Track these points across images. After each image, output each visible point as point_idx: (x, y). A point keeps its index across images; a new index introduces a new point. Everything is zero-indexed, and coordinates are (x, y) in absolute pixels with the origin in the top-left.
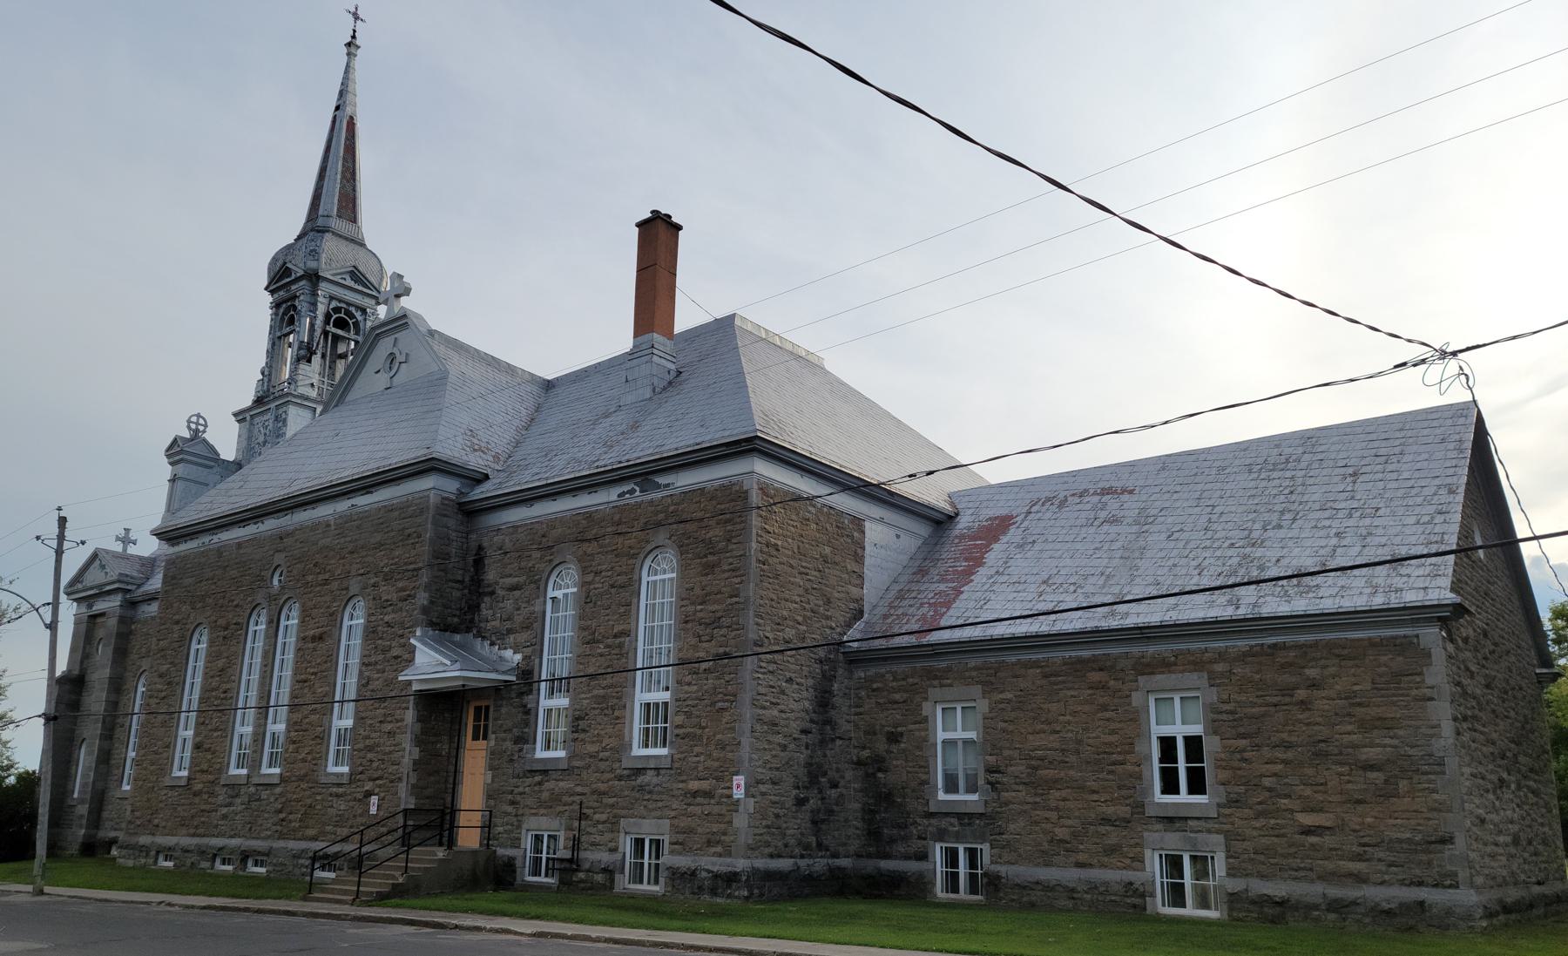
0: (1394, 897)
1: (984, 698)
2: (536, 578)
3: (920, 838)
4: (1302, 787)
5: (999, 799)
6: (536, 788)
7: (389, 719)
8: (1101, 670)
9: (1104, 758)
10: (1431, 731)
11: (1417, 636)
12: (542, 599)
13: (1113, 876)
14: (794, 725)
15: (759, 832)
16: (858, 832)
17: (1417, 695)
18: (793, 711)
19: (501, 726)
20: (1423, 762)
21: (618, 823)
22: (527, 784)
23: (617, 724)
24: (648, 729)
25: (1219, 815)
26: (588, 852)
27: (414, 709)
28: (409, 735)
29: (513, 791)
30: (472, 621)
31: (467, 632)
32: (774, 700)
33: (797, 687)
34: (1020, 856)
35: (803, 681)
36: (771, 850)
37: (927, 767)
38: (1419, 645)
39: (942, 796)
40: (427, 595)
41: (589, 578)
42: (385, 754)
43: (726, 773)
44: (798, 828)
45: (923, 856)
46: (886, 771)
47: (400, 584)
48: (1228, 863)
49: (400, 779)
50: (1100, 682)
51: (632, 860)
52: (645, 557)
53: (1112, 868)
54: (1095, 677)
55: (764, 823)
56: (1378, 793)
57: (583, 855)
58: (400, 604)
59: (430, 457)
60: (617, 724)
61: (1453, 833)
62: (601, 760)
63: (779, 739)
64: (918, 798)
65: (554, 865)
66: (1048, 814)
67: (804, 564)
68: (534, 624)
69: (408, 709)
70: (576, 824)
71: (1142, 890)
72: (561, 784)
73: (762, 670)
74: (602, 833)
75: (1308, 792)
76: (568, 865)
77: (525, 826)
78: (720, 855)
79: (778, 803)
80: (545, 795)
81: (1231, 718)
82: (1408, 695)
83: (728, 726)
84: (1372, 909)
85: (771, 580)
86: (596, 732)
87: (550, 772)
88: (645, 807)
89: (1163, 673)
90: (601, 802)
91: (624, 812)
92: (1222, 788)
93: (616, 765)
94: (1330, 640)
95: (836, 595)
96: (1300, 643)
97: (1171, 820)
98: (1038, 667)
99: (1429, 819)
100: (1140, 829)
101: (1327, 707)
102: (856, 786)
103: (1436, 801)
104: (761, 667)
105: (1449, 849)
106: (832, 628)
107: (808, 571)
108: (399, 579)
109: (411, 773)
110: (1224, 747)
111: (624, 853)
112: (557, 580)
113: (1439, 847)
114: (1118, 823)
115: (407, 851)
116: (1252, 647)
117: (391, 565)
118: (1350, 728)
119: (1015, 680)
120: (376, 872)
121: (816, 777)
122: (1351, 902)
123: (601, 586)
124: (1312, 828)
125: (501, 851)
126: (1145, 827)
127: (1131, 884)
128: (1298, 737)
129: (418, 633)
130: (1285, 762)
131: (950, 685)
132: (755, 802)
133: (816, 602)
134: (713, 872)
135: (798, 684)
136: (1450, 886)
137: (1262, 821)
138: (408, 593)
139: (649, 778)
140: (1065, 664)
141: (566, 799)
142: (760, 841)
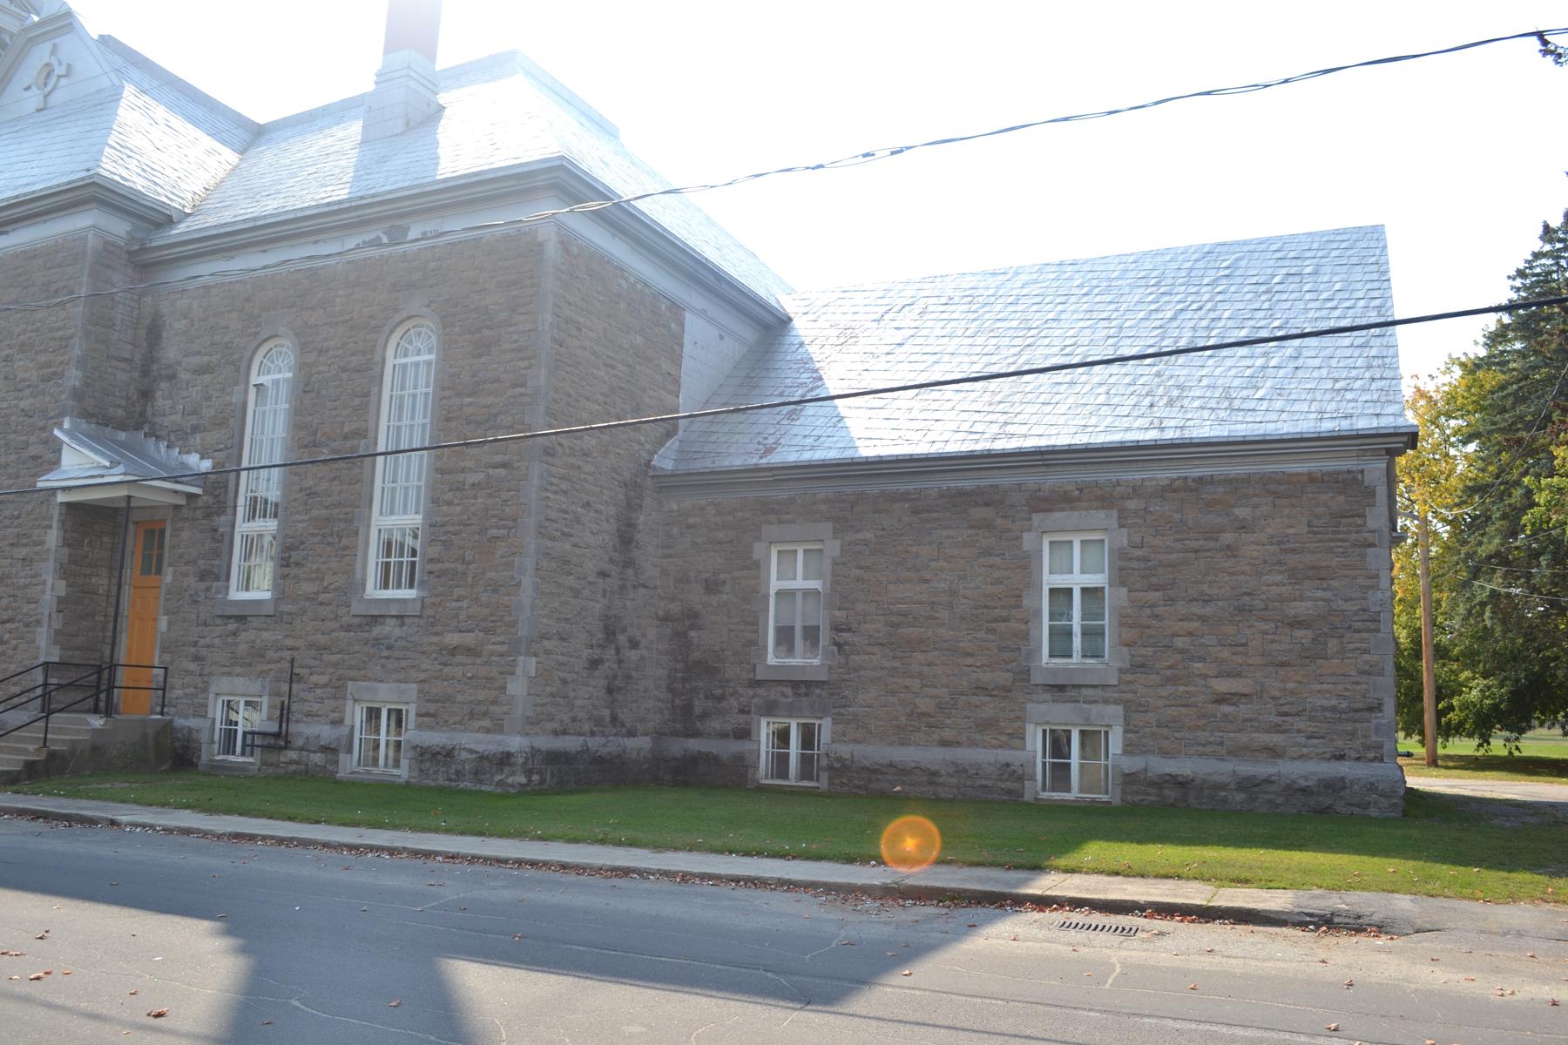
0: (1312, 774)
1: (835, 538)
2: (236, 357)
3: (742, 711)
4: (1220, 648)
5: (847, 664)
6: (230, 640)
7: (24, 541)
8: (987, 505)
9: (983, 614)
10: (1368, 582)
11: (1362, 472)
12: (242, 386)
13: (985, 756)
14: (590, 565)
15: (541, 702)
16: (660, 704)
17: (1357, 540)
18: (588, 547)
19: (181, 557)
20: (1356, 618)
21: (344, 687)
22: (216, 634)
23: (344, 556)
24: (388, 564)
25: (1119, 682)
26: (302, 724)
27: (58, 529)
28: (51, 564)
29: (197, 642)
30: (142, 414)
31: (136, 429)
32: (566, 530)
33: (594, 515)
34: (870, 732)
35: (603, 508)
36: (556, 725)
37: (756, 624)
38: (1363, 481)
39: (771, 660)
40: (79, 373)
41: (311, 358)
42: (19, 588)
43: (499, 624)
44: (589, 698)
45: (744, 733)
46: (700, 629)
47: (42, 358)
48: (1125, 738)
49: (38, 622)
50: (985, 519)
51: (363, 736)
52: (392, 332)
53: (985, 747)
54: (979, 513)
55: (548, 689)
56: (1303, 654)
57: (293, 728)
58: (42, 386)
59: (91, 181)
60: (344, 556)
61: (1382, 699)
62: (321, 604)
63: (570, 581)
64: (742, 662)
65: (253, 740)
66: (908, 682)
67: (611, 354)
68: (231, 422)
69: (51, 527)
70: (285, 688)
71: (1021, 772)
72: (265, 635)
73: (553, 488)
74: (321, 700)
75: (1225, 653)
76: (272, 741)
77: (213, 689)
78: (488, 731)
79: (565, 665)
80: (242, 649)
81: (1143, 566)
82: (1345, 541)
83: (504, 560)
84: (1288, 787)
85: (569, 369)
86: (315, 567)
87: (249, 619)
88: (383, 666)
89: (1062, 510)
90: (321, 660)
91: (352, 673)
92: (1125, 650)
93: (341, 612)
94: (1265, 474)
95: (647, 400)
96: (1231, 477)
97: (1061, 688)
98: (908, 500)
99: (1357, 683)
100: (1022, 700)
101: (1255, 553)
102: (660, 647)
103: (1367, 662)
104: (552, 484)
105: (1376, 718)
106: (640, 443)
107: (615, 363)
108: (41, 352)
109: (54, 615)
110: (1131, 601)
111: (353, 727)
112: (265, 361)
113: (1367, 715)
114: (995, 693)
115: (47, 717)
116: (1173, 480)
117: (31, 332)
118: (1279, 578)
119: (877, 516)
120: (23, 734)
121: (614, 633)
122: (1264, 780)
123: (327, 368)
124: (1228, 696)
125: (179, 722)
126: (1028, 697)
127: (1007, 765)
128: (1220, 588)
129: (66, 425)
130: (1203, 619)
131: (793, 522)
132: (538, 663)
133: (623, 406)
134: (478, 752)
135: (596, 511)
136: (1374, 760)
137: (1169, 689)
138: (53, 369)
139: (390, 629)
140: (942, 497)
141: (271, 654)
142: (543, 713)
